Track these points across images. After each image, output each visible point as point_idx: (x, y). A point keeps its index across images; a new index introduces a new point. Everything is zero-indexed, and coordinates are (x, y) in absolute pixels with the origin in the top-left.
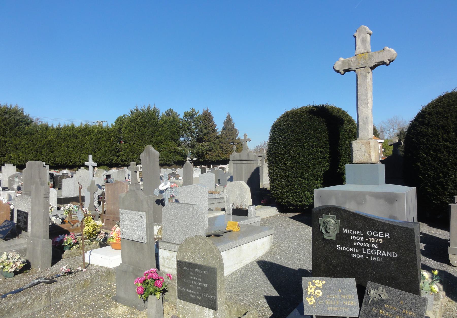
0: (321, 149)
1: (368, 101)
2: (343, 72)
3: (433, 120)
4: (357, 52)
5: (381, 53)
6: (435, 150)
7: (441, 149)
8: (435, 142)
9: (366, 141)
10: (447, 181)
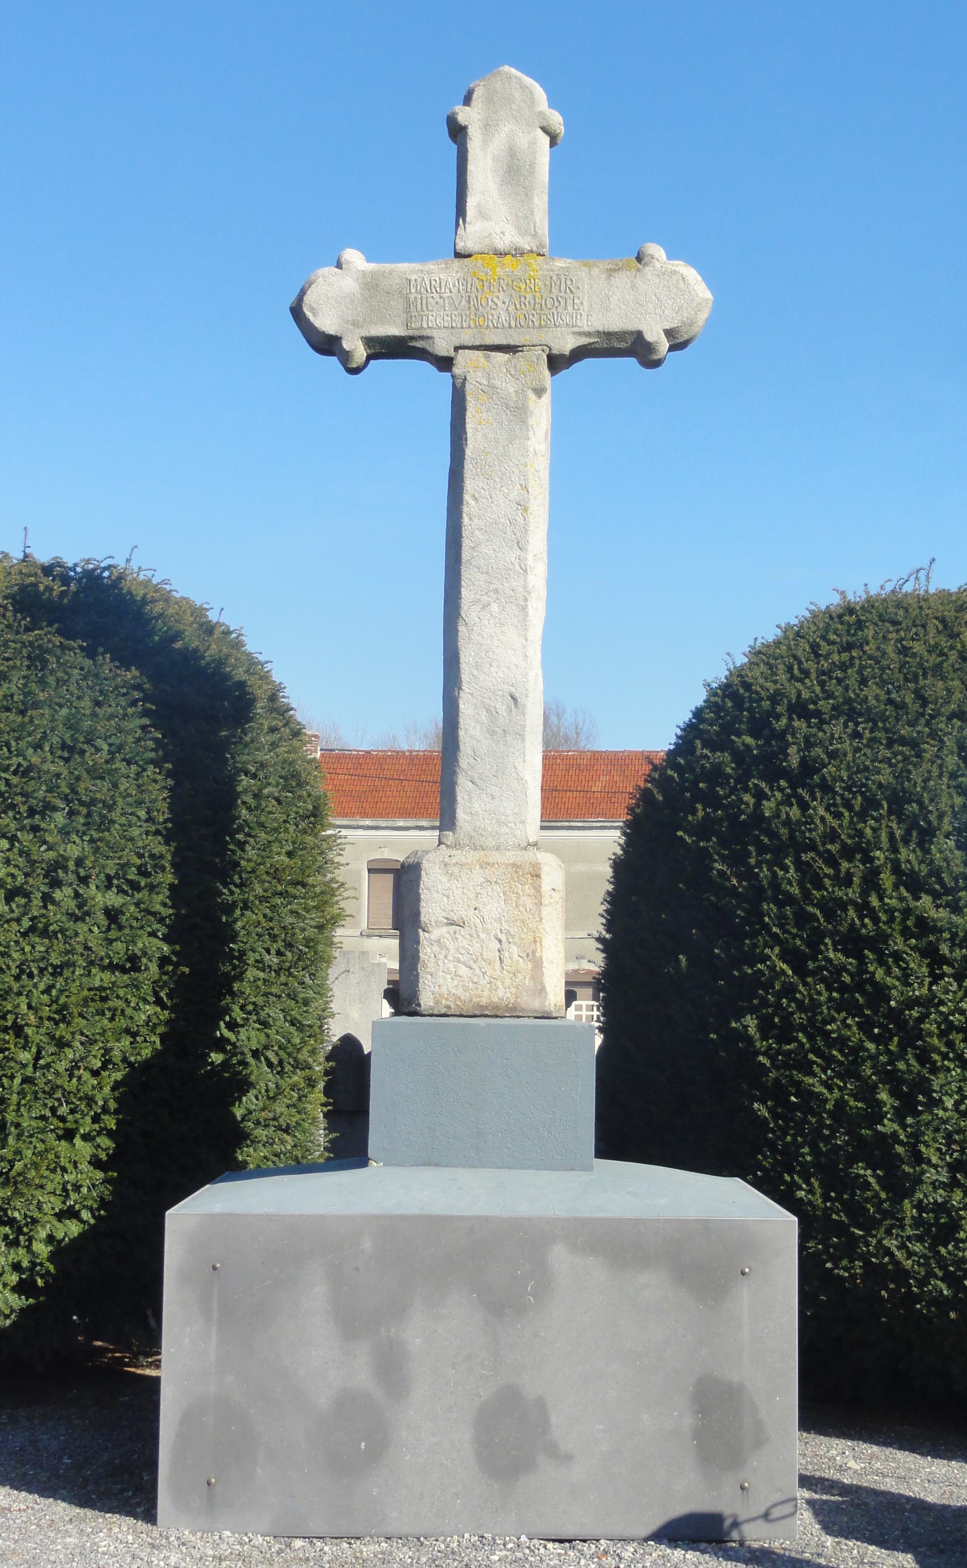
0: (113, 899)
1: (531, 579)
2: (360, 353)
3: (832, 755)
4: (472, 235)
5: (622, 280)
6: (853, 943)
7: (885, 938)
8: (853, 893)
9: (512, 856)
10: (916, 1137)
